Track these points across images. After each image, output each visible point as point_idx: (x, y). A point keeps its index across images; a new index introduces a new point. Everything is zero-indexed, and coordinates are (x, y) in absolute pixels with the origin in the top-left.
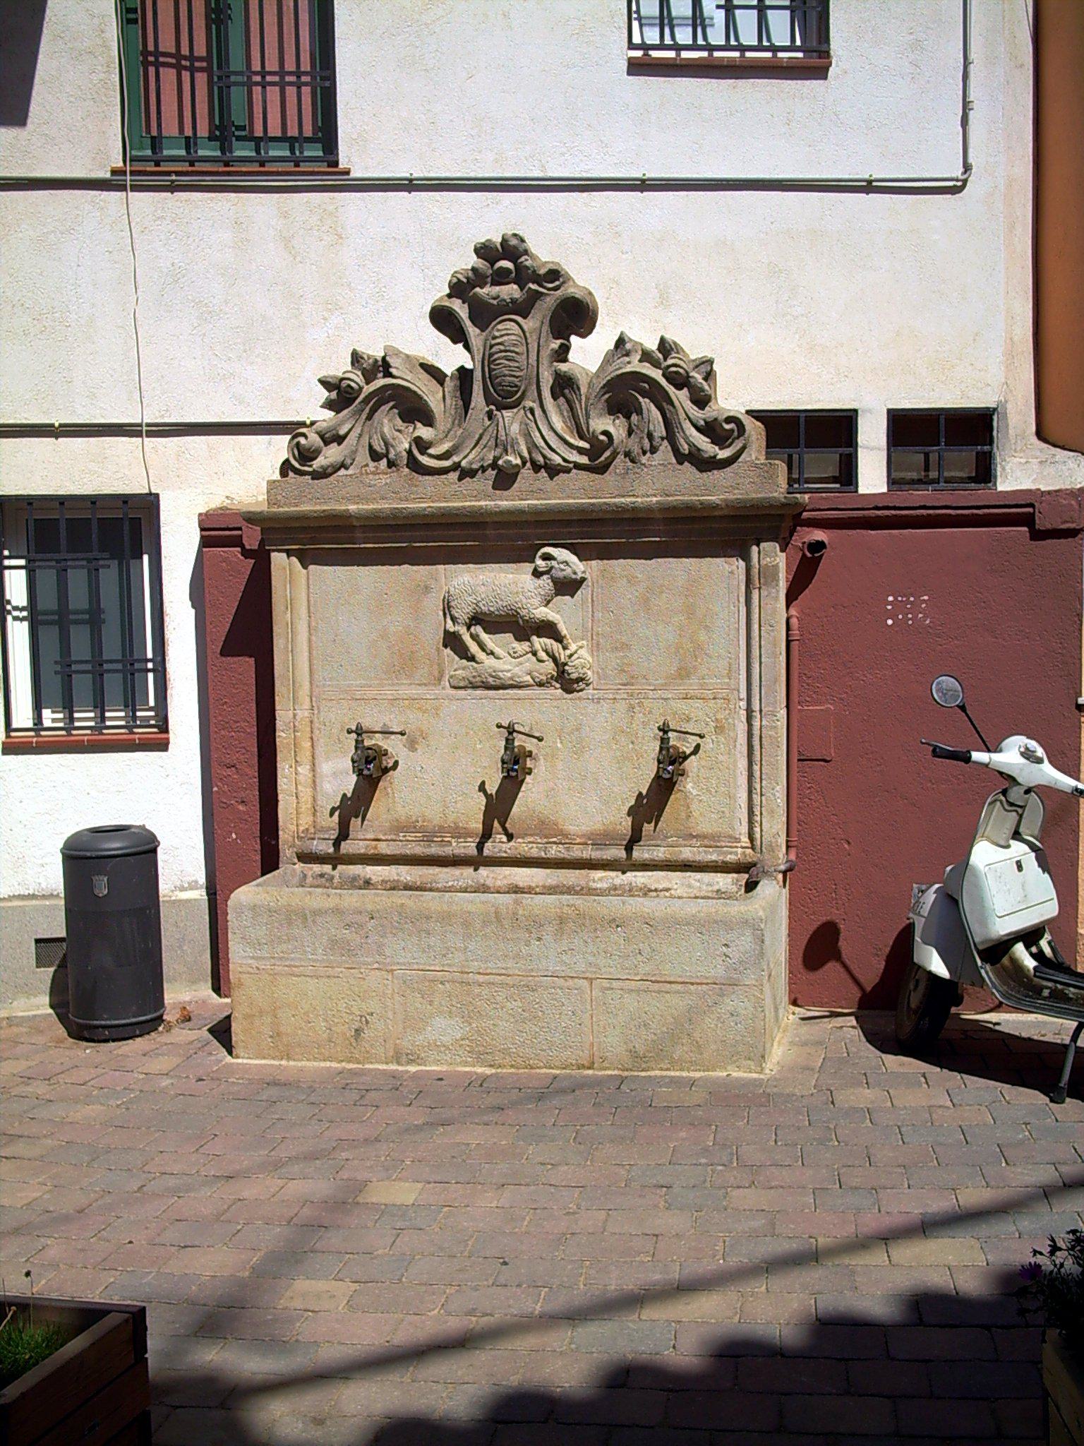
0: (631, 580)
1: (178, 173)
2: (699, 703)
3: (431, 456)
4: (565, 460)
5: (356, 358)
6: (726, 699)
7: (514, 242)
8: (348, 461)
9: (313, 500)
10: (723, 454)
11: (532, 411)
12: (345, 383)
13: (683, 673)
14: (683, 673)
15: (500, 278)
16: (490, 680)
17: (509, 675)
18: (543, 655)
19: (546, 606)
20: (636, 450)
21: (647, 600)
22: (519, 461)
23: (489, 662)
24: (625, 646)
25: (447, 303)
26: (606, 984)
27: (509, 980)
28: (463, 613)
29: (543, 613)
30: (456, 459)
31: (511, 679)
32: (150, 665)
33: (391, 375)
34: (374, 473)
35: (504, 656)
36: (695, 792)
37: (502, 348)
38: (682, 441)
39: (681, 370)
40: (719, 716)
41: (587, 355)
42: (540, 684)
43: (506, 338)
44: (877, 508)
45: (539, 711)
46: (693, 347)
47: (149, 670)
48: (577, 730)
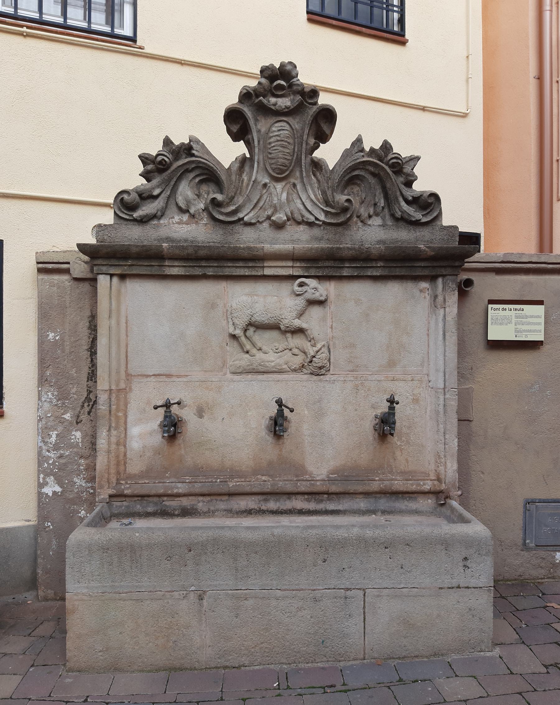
0: (358, 302)
1: (28, 27)
2: (401, 384)
3: (222, 213)
4: (317, 219)
5: (167, 142)
6: (420, 381)
7: (289, 67)
8: (159, 213)
9: (133, 235)
10: (424, 220)
11: (294, 185)
12: (160, 158)
13: (392, 364)
14: (392, 364)
15: (276, 92)
16: (260, 367)
17: (273, 364)
18: (296, 351)
19: (299, 318)
20: (365, 215)
21: (367, 315)
22: (285, 218)
23: (259, 356)
24: (353, 346)
25: (240, 106)
26: (375, 592)
27: (300, 594)
28: (242, 321)
29: (297, 323)
30: (241, 215)
31: (273, 367)
32: (395, 9)
33: (193, 155)
34: (179, 223)
35: (270, 350)
36: (399, 443)
37: (279, 138)
38: (397, 210)
39: (400, 161)
40: (415, 392)
41: (330, 153)
42: (295, 370)
43: (282, 132)
44: (503, 262)
45: (296, 389)
46: (402, 149)
47: (395, 11)
48: (319, 401)
